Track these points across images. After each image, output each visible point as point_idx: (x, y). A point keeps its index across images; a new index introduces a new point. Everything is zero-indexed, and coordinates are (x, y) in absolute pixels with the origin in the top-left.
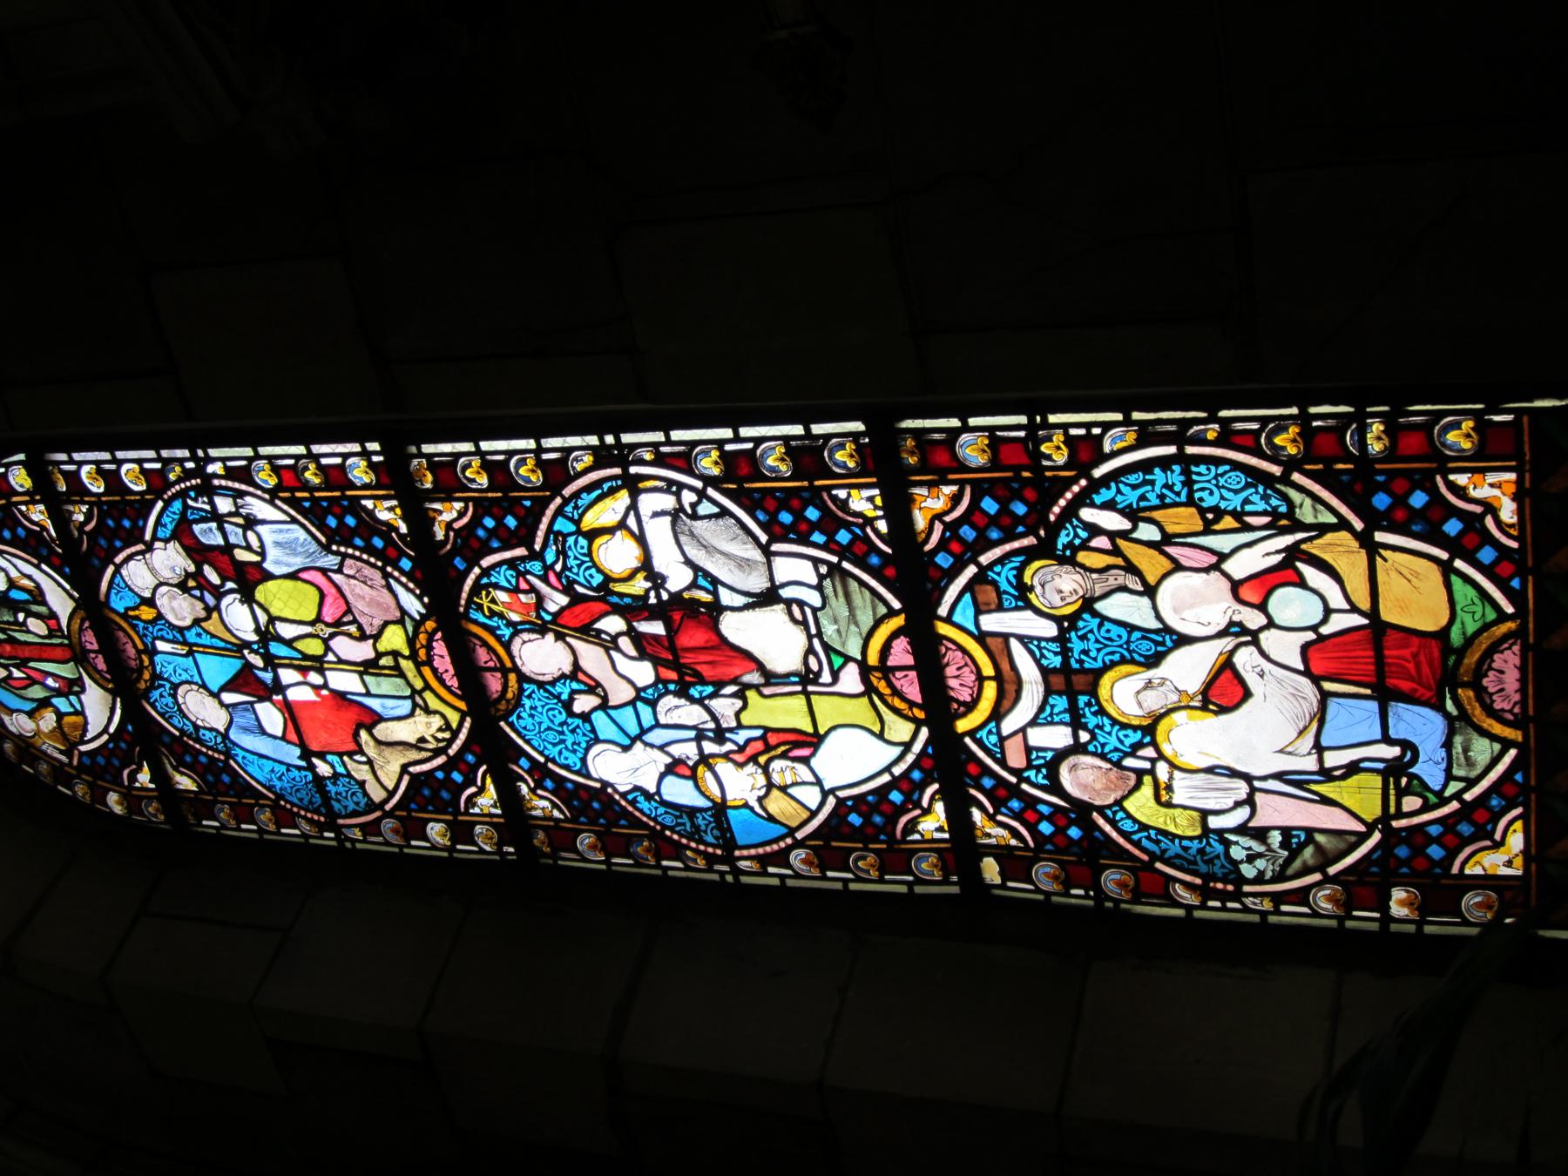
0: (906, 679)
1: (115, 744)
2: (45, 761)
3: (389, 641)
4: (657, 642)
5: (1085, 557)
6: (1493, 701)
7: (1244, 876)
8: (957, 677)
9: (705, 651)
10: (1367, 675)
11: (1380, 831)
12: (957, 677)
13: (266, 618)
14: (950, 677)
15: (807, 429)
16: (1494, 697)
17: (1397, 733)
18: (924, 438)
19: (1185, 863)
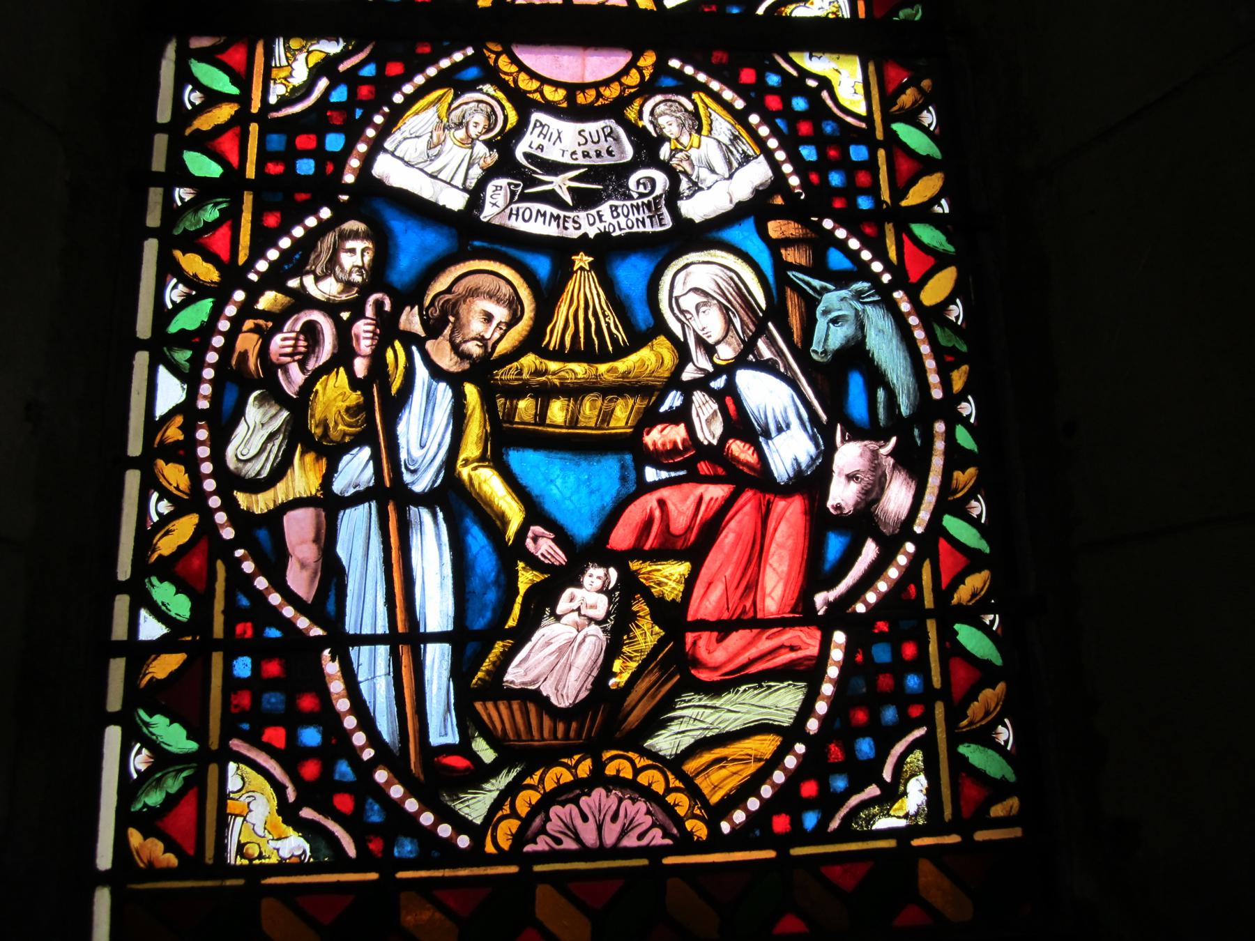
0: (610, 813)
1: (245, 610)
2: (375, 457)
3: (681, 513)
4: (747, 588)
5: (255, 108)
6: (563, 804)
7: (144, 340)
8: (600, 828)
9: (709, 592)
10: (758, 425)
11: (794, 187)
12: (600, 828)
13: (752, 615)
14: (607, 571)
15: (163, 128)
16: (648, 820)
17: (119, 600)
18: (856, 269)
19: (261, 322)
